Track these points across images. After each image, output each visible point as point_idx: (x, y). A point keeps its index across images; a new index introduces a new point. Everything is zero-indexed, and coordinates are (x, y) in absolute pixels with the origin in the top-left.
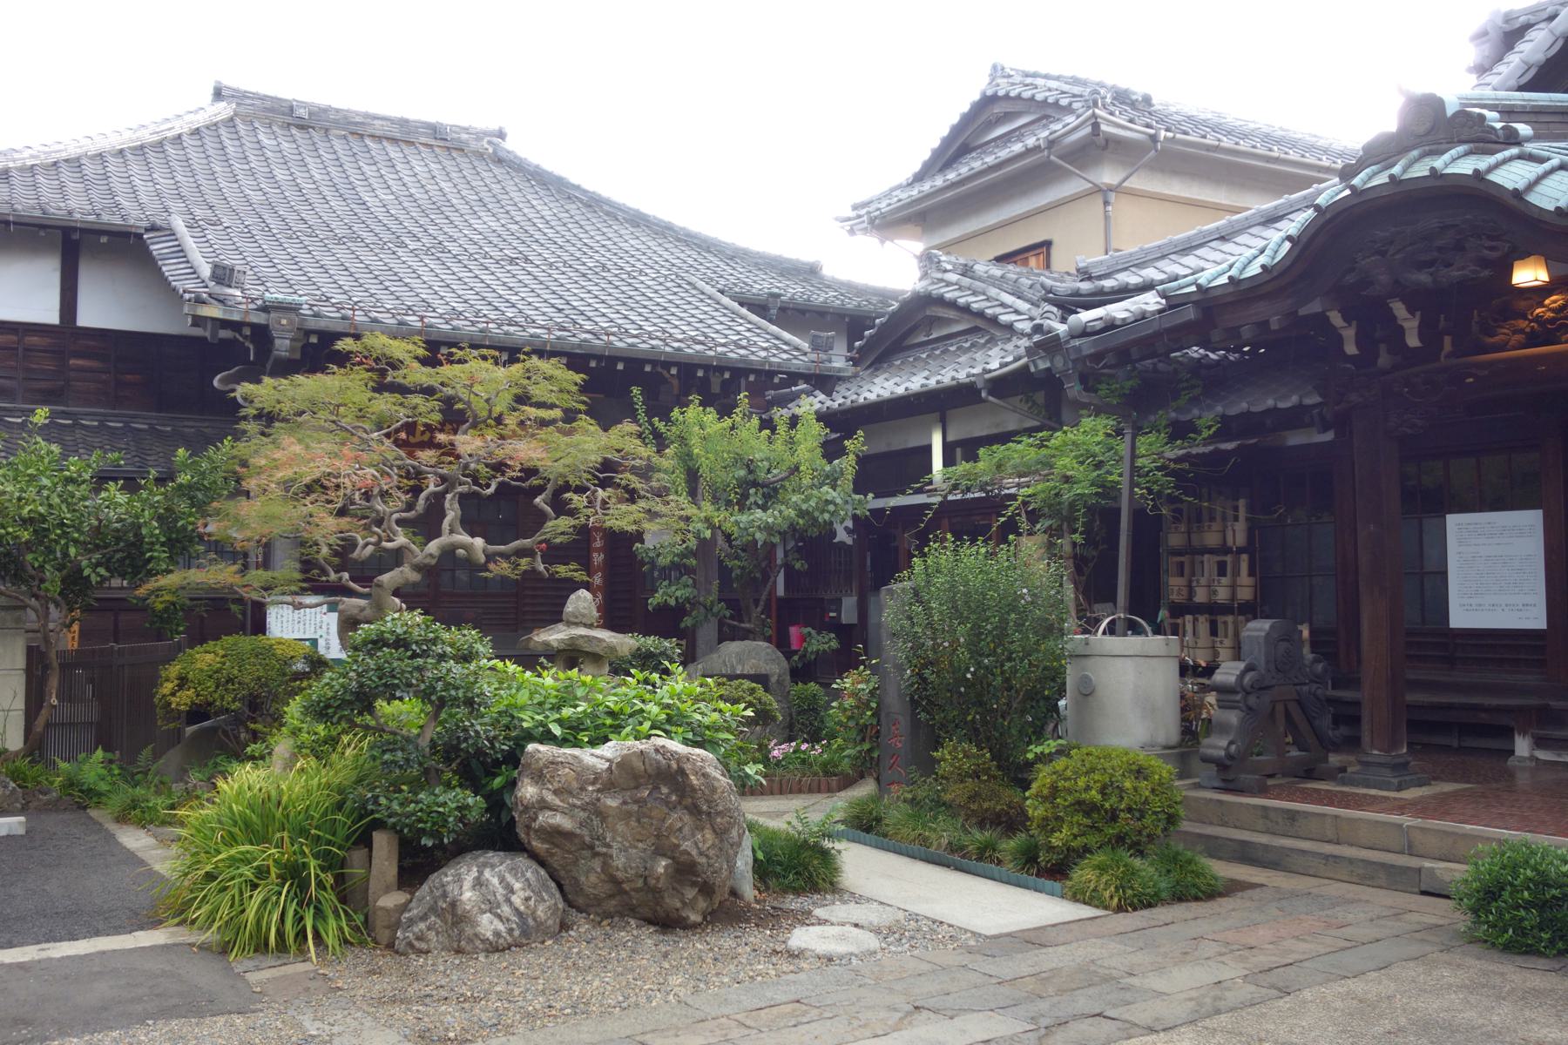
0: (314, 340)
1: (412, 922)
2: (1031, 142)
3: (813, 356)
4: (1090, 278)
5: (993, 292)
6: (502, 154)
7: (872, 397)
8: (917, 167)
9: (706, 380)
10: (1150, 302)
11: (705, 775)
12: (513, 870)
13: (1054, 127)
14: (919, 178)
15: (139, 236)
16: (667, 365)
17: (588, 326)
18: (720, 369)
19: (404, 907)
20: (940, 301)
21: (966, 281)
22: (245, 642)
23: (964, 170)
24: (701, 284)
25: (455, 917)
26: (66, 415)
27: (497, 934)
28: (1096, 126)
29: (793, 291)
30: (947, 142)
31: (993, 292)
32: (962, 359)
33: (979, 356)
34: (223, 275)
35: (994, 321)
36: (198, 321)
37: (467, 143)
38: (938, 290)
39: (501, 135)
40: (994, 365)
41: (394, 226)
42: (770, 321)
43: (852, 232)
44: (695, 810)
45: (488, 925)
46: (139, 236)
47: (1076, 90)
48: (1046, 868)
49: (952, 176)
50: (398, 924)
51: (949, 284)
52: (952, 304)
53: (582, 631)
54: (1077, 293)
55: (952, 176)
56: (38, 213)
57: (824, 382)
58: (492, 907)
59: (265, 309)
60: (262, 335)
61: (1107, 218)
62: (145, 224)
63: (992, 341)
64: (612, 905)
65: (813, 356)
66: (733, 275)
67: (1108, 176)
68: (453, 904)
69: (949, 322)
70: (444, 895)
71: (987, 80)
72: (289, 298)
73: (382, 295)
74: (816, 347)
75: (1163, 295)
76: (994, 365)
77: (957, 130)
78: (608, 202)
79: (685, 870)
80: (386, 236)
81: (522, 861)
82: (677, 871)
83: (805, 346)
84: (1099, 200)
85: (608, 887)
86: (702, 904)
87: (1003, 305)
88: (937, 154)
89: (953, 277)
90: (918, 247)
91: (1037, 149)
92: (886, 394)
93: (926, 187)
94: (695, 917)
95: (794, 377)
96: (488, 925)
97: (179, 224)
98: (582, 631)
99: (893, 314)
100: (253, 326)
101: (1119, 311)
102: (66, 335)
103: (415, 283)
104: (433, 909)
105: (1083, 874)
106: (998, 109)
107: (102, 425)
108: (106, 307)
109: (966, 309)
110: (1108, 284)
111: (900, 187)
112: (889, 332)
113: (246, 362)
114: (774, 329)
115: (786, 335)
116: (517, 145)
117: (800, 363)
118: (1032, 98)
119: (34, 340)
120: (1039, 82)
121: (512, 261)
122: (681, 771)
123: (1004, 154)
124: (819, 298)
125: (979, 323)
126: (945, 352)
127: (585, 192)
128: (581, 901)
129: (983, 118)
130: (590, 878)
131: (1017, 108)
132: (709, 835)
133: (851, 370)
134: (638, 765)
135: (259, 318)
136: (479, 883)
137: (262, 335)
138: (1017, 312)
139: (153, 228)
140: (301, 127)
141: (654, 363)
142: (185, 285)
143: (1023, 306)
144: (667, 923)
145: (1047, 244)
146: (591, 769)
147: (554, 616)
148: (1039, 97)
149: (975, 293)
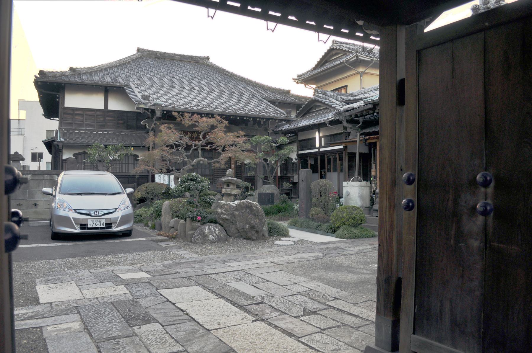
0: (165, 112)
1: (195, 236)
2: (342, 61)
3: (286, 115)
4: (353, 96)
5: (331, 99)
6: (208, 63)
7: (301, 125)
8: (314, 66)
9: (260, 121)
10: (361, 103)
11: (257, 207)
12: (216, 227)
13: (347, 57)
14: (314, 69)
15: (123, 88)
16: (250, 118)
17: (230, 108)
18: (263, 119)
19: (194, 234)
20: (318, 101)
21: (324, 96)
22: (149, 185)
23: (325, 68)
24: (258, 97)
25: (205, 236)
26: (106, 131)
27: (213, 239)
28: (357, 57)
29: (282, 98)
30: (321, 60)
31: (331, 99)
32: (323, 116)
33: (327, 115)
34: (145, 98)
35: (331, 106)
36: (138, 108)
37: (199, 61)
38: (317, 99)
39: (208, 58)
40: (330, 117)
41: (182, 83)
42: (276, 106)
43: (297, 83)
44: (254, 215)
45: (211, 237)
46: (123, 88)
47: (353, 47)
48: (333, 231)
49: (322, 69)
50: (192, 237)
51: (320, 97)
52: (321, 102)
53: (230, 178)
54: (350, 100)
55: (322, 69)
56: (100, 83)
57: (288, 121)
58: (212, 234)
59: (154, 105)
60: (153, 112)
61: (361, 80)
62: (124, 85)
63: (330, 111)
64: (236, 235)
65: (286, 115)
66: (267, 94)
67: (361, 70)
68: (204, 233)
69: (320, 106)
70: (202, 231)
71: (331, 44)
72: (160, 103)
73: (181, 101)
74: (287, 113)
75: (364, 102)
76: (330, 117)
77: (324, 57)
78: (235, 75)
79: (252, 227)
80: (181, 86)
81: (218, 225)
82: (251, 228)
83: (284, 112)
84: (359, 76)
85: (236, 231)
86: (256, 235)
87: (333, 102)
88: (319, 63)
89: (321, 95)
90: (314, 86)
91: (343, 63)
92: (304, 125)
93: (316, 71)
94: (254, 238)
95: (282, 120)
96: (211, 237)
97: (131, 84)
98: (230, 178)
99: (307, 104)
100: (151, 109)
101: (355, 105)
102: (106, 111)
103: (188, 98)
104: (200, 234)
105: (339, 232)
106: (334, 52)
107: (114, 133)
108: (116, 105)
109: (324, 103)
110: (357, 98)
111: (309, 71)
112: (306, 107)
113: (149, 118)
114: (277, 108)
115: (280, 110)
116: (213, 60)
117: (283, 117)
118: (342, 49)
119: (98, 113)
120: (344, 45)
121: (211, 92)
122: (251, 206)
123: (335, 64)
124: (289, 100)
125: (327, 107)
126: (319, 114)
127: (229, 73)
128: (230, 234)
129: (331, 54)
130: (232, 229)
131: (339, 52)
132: (258, 220)
133: (296, 119)
134: (242, 205)
135: (152, 108)
136: (209, 229)
137: (153, 112)
138: (336, 104)
139: (126, 86)
140: (158, 58)
141: (247, 117)
142: (135, 100)
143: (338, 102)
144: (249, 239)
145: (346, 86)
146: (233, 206)
147: (224, 175)
148: (344, 49)
149: (326, 99)
